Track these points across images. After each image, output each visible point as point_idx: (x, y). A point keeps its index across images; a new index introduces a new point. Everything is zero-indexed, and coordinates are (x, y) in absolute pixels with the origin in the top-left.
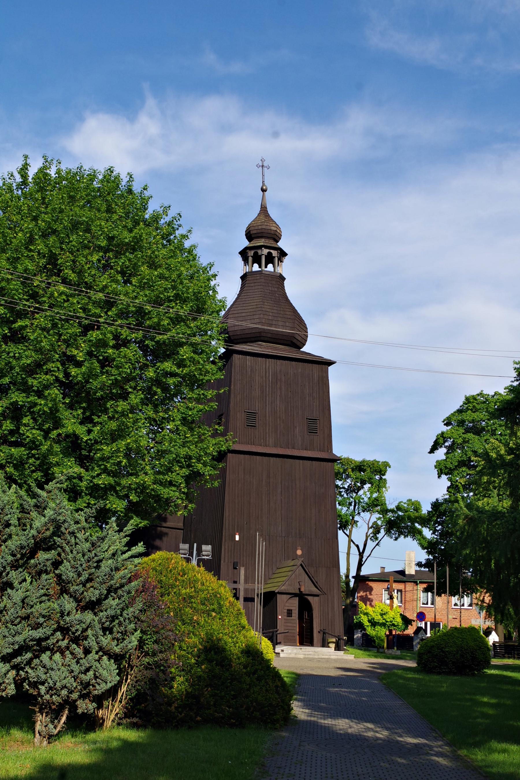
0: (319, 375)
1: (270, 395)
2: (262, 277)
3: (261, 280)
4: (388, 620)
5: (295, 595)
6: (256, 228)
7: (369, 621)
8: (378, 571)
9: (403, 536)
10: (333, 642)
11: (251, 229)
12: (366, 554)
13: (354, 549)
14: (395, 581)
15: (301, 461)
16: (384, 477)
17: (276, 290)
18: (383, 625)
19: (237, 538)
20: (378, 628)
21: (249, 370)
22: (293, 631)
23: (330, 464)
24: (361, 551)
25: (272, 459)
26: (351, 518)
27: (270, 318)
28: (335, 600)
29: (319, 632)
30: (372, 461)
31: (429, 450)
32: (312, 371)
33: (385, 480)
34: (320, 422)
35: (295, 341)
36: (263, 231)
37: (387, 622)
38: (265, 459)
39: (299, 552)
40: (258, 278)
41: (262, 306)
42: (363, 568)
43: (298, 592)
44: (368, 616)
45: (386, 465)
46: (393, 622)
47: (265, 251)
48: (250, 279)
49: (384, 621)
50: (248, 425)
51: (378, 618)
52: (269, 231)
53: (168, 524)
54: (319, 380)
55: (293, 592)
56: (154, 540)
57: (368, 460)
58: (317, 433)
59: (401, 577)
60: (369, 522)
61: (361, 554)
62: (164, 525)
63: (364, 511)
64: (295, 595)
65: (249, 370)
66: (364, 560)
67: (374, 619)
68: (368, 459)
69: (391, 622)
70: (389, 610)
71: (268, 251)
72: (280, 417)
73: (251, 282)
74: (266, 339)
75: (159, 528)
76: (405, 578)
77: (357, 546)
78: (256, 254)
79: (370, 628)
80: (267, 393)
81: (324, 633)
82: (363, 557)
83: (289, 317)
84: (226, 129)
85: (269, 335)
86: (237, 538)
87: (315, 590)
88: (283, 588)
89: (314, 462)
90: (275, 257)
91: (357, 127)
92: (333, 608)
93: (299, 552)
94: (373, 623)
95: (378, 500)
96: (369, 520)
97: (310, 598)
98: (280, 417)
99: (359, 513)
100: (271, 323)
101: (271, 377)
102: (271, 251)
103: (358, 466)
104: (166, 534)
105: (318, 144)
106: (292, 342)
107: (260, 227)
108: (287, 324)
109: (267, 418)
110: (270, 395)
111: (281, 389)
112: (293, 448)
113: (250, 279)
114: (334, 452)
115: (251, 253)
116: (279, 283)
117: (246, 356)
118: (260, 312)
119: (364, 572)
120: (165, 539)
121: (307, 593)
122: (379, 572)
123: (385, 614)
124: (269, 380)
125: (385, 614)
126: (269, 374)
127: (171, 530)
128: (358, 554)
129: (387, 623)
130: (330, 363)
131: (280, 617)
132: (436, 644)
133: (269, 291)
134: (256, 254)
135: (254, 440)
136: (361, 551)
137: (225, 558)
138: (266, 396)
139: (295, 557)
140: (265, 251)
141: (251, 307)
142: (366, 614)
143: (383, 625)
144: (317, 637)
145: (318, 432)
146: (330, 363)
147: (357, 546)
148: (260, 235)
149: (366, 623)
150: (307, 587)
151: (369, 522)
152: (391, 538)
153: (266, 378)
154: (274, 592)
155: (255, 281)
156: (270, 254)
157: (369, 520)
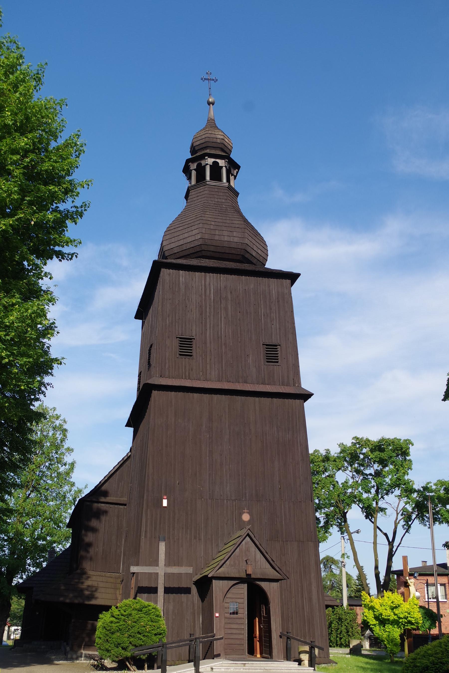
0: (278, 292)
1: (212, 317)
2: (206, 189)
3: (205, 192)
4: (402, 616)
5: (241, 580)
6: (200, 138)
7: (376, 618)
8: (420, 565)
9: (438, 523)
10: (305, 652)
11: (194, 145)
12: (396, 544)
13: (382, 539)
14: (439, 575)
15: (257, 399)
16: (408, 458)
17: (224, 201)
18: (395, 623)
19: (165, 503)
20: (389, 627)
21: (182, 287)
22: (241, 637)
23: (298, 401)
24: (391, 540)
25: (216, 397)
26: (374, 503)
27: (212, 227)
28: (313, 588)
29: (281, 637)
30: (393, 439)
31: (443, 397)
32: (269, 286)
33: (410, 461)
34: (281, 349)
35: (247, 256)
36: (207, 140)
37: (400, 618)
38: (206, 397)
39: (246, 517)
40: (202, 190)
41: (203, 215)
42: (394, 558)
43: (244, 576)
44: (374, 612)
45: (408, 442)
46: (409, 618)
47: (210, 161)
48: (193, 193)
49: (396, 617)
50: (180, 355)
51: (387, 613)
52: (215, 140)
53: (108, 499)
54: (278, 298)
55: (237, 575)
56: (90, 520)
57: (387, 438)
58: (277, 362)
59: (442, 570)
60: (397, 508)
61: (391, 544)
62: (103, 499)
63: (387, 494)
64: (241, 580)
65: (182, 287)
66: (394, 549)
67: (381, 614)
68: (387, 437)
69: (406, 618)
70: (402, 602)
71: (213, 160)
72: (225, 344)
73: (194, 196)
74: (208, 254)
75: (96, 505)
76: (447, 571)
77: (386, 535)
78: (199, 165)
79: (378, 627)
80: (208, 314)
81: (286, 637)
82: (393, 547)
83: (237, 226)
84: (294, 242)
85: (212, 249)
86: (165, 503)
87: (273, 574)
88: (222, 571)
89: (275, 400)
90: (222, 167)
91: (394, 230)
92: (310, 599)
93: (246, 517)
94: (383, 622)
95: (400, 480)
96: (398, 506)
97: (263, 585)
98: (225, 344)
99: (382, 497)
100: (213, 233)
101: (212, 295)
102: (217, 160)
103: (377, 446)
104: (105, 512)
105: (364, 247)
106: (243, 256)
107: (203, 137)
108: (235, 234)
109: (208, 345)
110: (212, 317)
111: (226, 309)
112: (246, 382)
113: (193, 193)
114: (303, 386)
115: (193, 166)
116: (228, 195)
117: (179, 270)
118: (198, 222)
119: (397, 565)
120: (103, 518)
121: (259, 576)
122: (421, 565)
123: (396, 607)
124: (210, 299)
125: (396, 607)
126: (210, 291)
127: (111, 506)
128: (387, 543)
129: (401, 621)
130: (293, 277)
131: (217, 615)
132: (433, 663)
133: (214, 202)
134: (199, 165)
135: (189, 374)
136: (391, 540)
137: (146, 532)
138: (206, 319)
139: (241, 525)
140: (210, 161)
141: (189, 219)
142: (372, 608)
143: (395, 623)
144: (277, 643)
145: (279, 360)
146: (293, 277)
147: (386, 535)
148: (204, 146)
149: (372, 621)
150: (259, 566)
151: (397, 508)
152: (425, 525)
153: (205, 296)
154: (206, 576)
155: (198, 194)
156: (215, 163)
157: (398, 506)
